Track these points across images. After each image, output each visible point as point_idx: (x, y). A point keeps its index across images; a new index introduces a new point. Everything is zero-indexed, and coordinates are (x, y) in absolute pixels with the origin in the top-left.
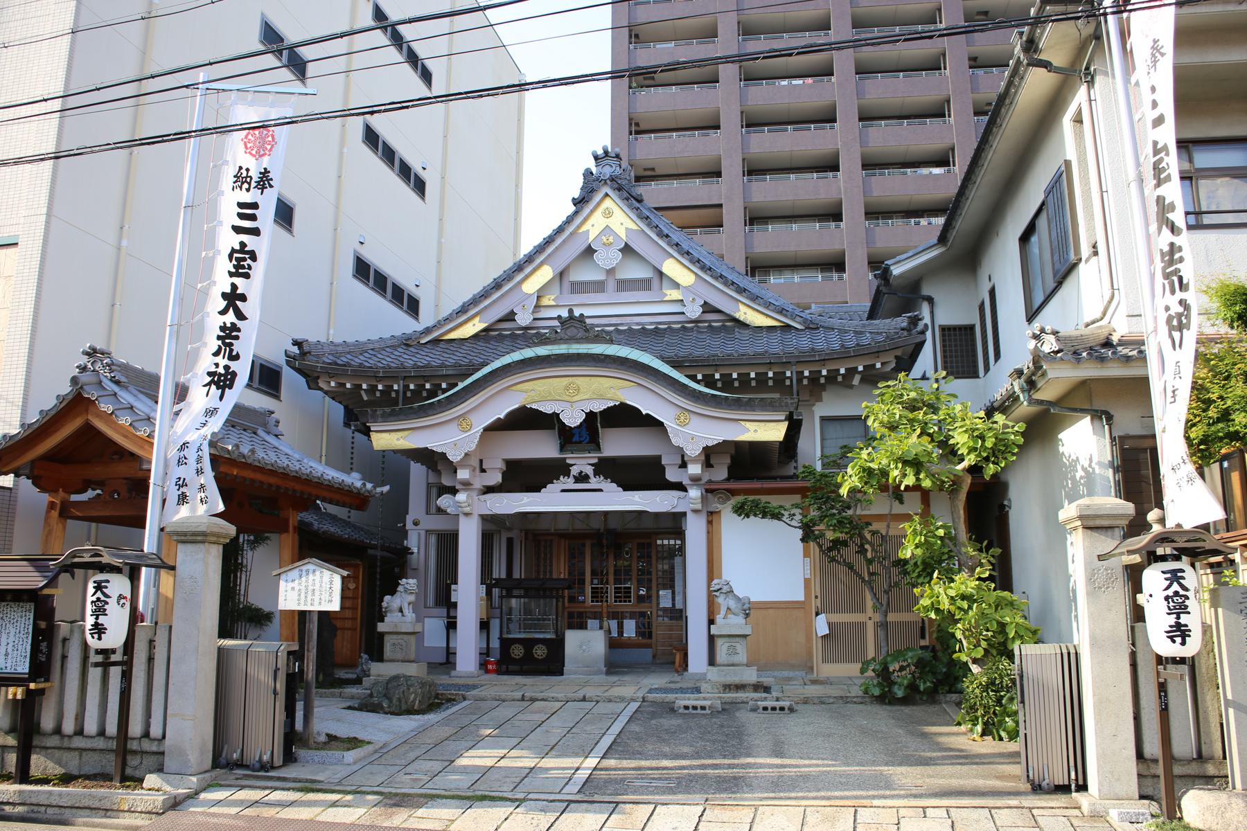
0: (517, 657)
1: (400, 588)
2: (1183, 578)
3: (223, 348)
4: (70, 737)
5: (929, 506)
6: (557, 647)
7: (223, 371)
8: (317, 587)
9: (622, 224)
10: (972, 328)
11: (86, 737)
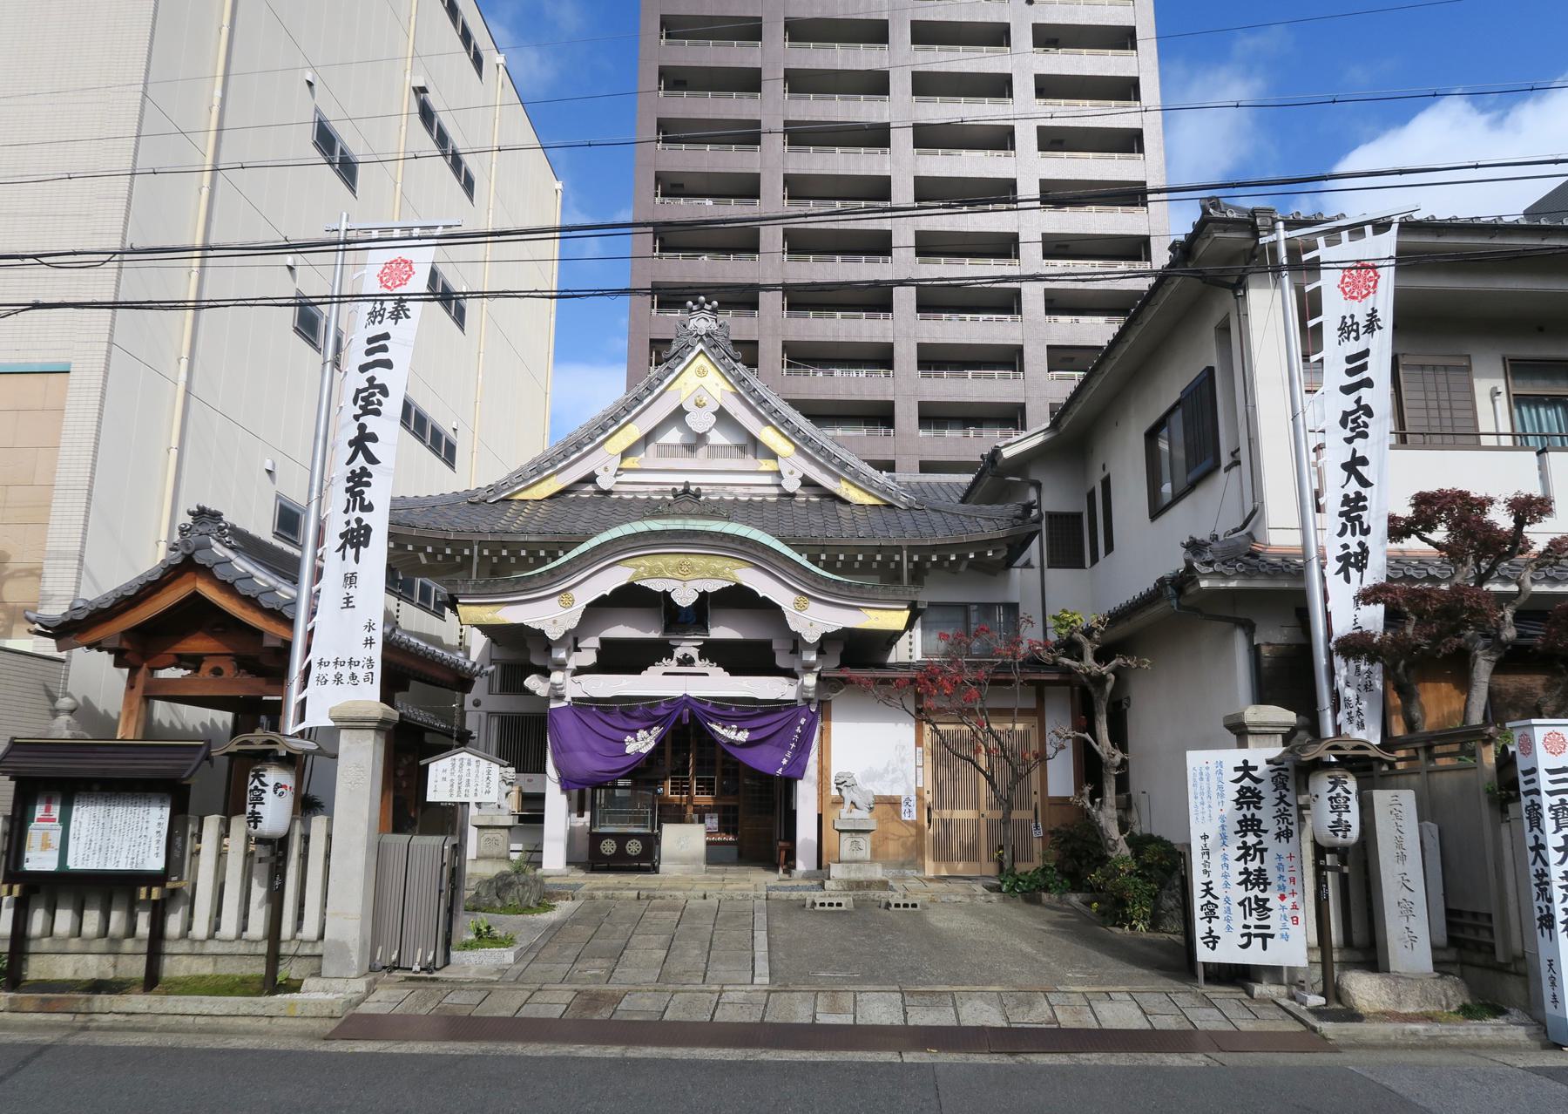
4: (202, 941)
5: (1043, 701)
6: (651, 844)
7: (355, 526)
8: (472, 778)
10: (1079, 516)
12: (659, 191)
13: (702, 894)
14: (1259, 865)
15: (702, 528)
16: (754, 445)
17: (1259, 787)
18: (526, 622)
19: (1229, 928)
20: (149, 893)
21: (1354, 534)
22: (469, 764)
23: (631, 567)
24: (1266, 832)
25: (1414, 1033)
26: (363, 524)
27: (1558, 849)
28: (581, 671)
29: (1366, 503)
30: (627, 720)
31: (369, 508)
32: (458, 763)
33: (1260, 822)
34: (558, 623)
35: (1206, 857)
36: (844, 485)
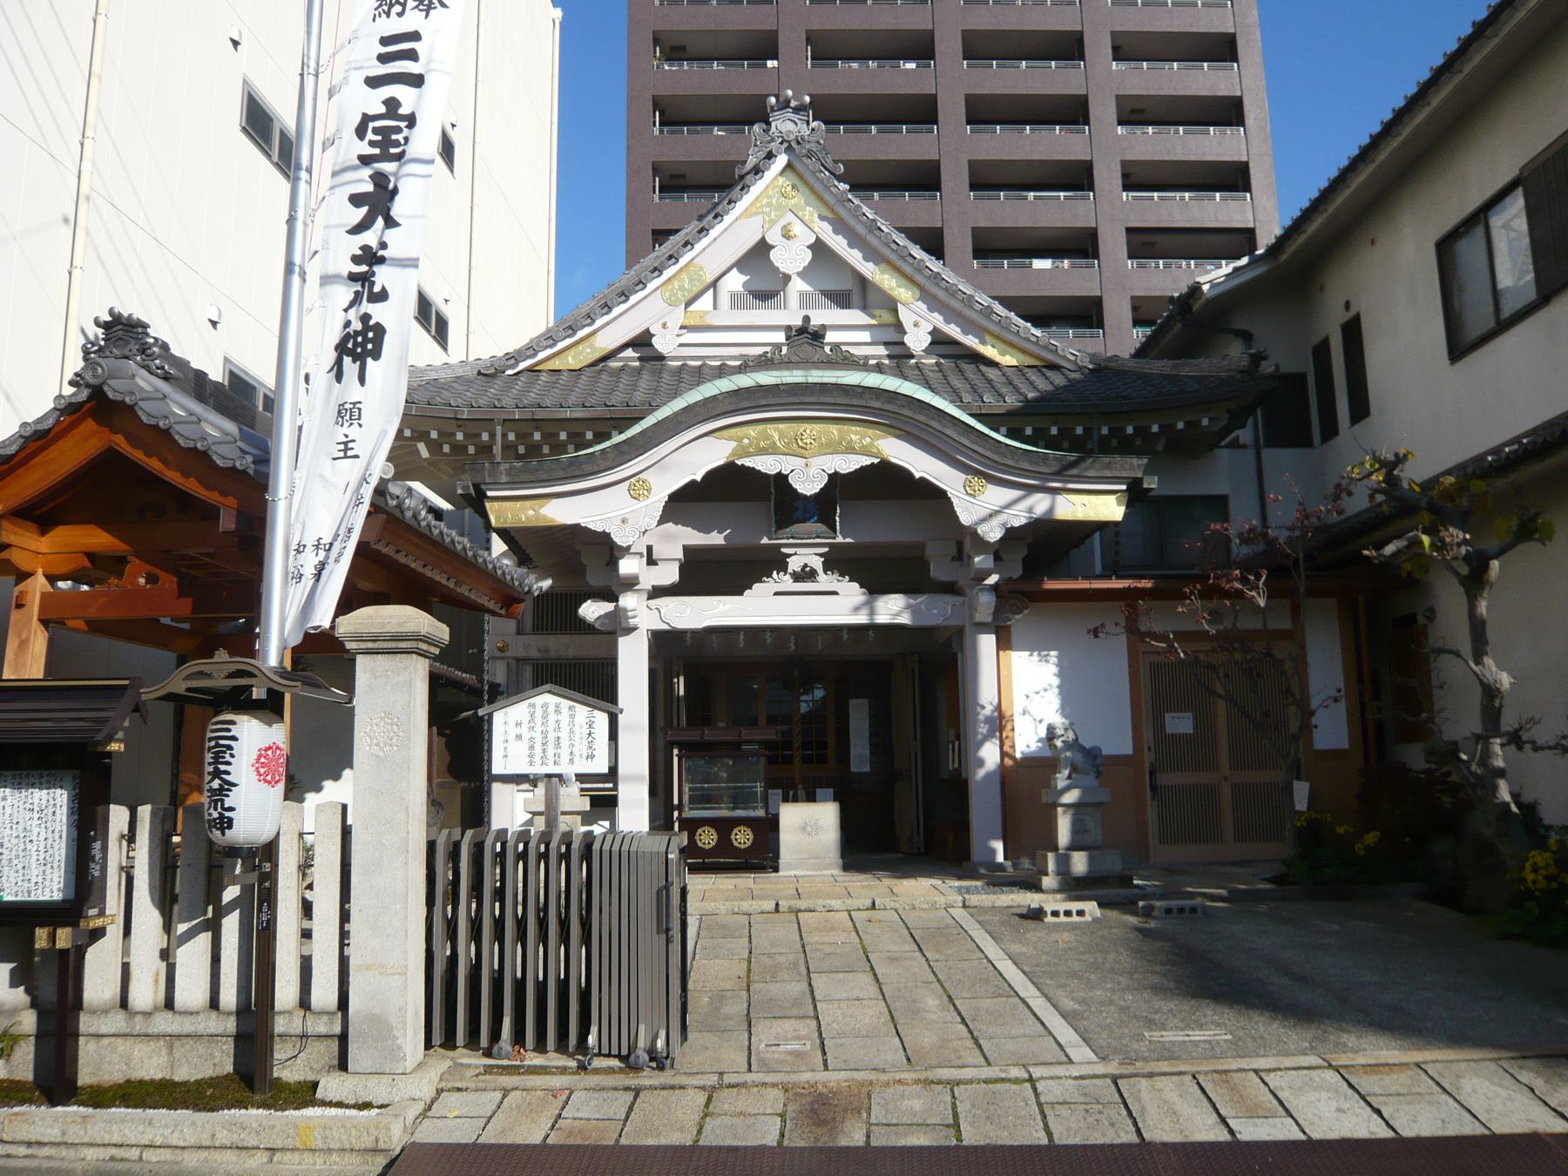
2: (228, 773)
4: (147, 1014)
6: (768, 829)
8: (564, 734)
11: (180, 1013)
13: (868, 903)
15: (833, 380)
18: (583, 522)
20: (52, 938)
22: (558, 711)
23: (729, 439)
26: (372, 323)
28: (657, 592)
31: (382, 296)
32: (539, 712)
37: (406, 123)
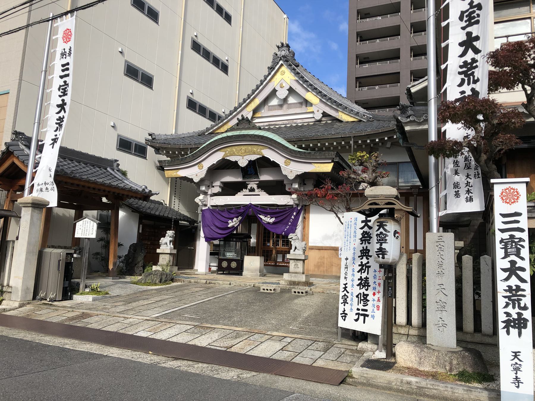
0: (233, 267)
1: (167, 235)
3: (59, 127)
8: (88, 228)
9: (289, 77)
12: (359, 18)
14: (367, 275)
16: (306, 103)
17: (371, 231)
18: (187, 176)
19: (351, 310)
21: (469, 84)
24: (371, 256)
25: (409, 383)
27: (505, 270)
29: (478, 64)
30: (229, 214)
32: (84, 222)
33: (369, 251)
34: (198, 176)
35: (346, 269)
36: (340, 113)
37: (476, 8)
